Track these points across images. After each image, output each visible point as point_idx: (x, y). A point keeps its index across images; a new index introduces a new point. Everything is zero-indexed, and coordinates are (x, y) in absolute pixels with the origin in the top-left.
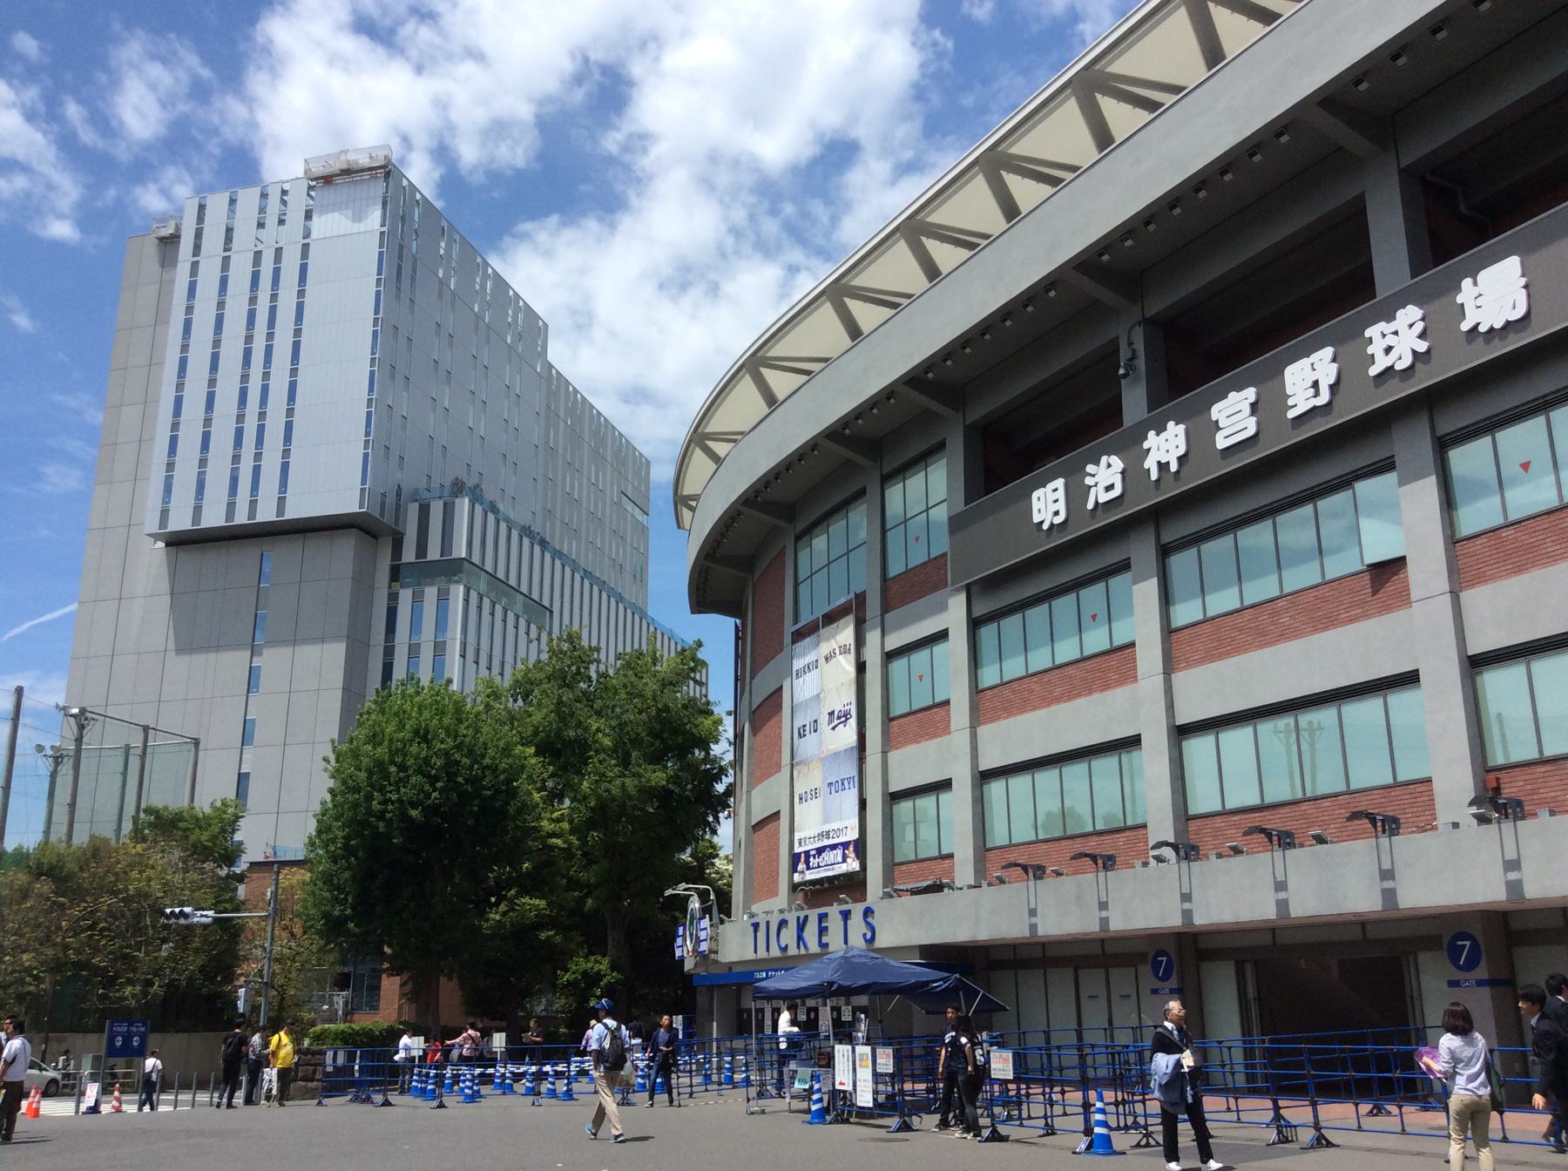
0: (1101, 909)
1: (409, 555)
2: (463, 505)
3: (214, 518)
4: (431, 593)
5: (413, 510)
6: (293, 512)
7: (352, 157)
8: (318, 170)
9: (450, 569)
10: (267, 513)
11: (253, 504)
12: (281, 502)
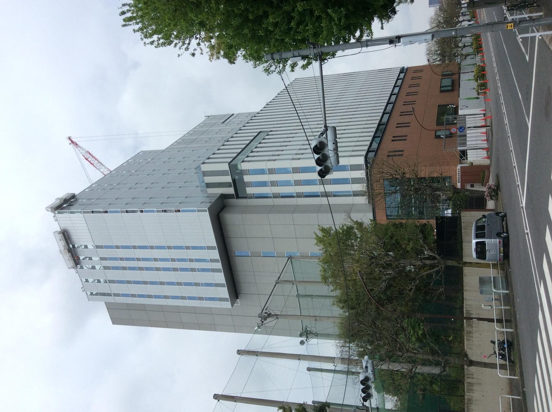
0: (85, 246)
1: (231, 191)
2: (205, 168)
3: (221, 278)
4: (247, 178)
5: (211, 191)
6: (212, 241)
7: (62, 248)
8: (72, 263)
9: (233, 168)
10: (215, 254)
11: (212, 261)
12: (209, 248)
